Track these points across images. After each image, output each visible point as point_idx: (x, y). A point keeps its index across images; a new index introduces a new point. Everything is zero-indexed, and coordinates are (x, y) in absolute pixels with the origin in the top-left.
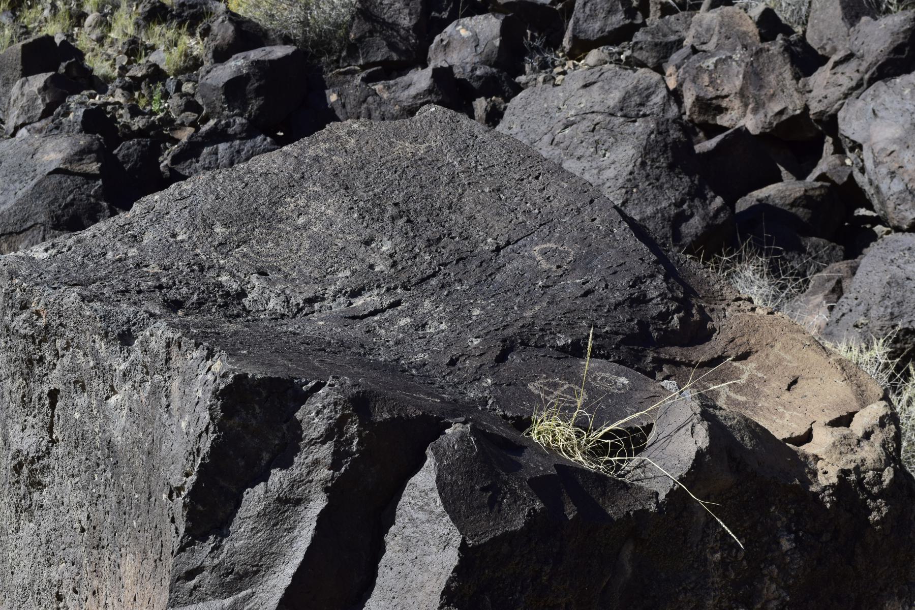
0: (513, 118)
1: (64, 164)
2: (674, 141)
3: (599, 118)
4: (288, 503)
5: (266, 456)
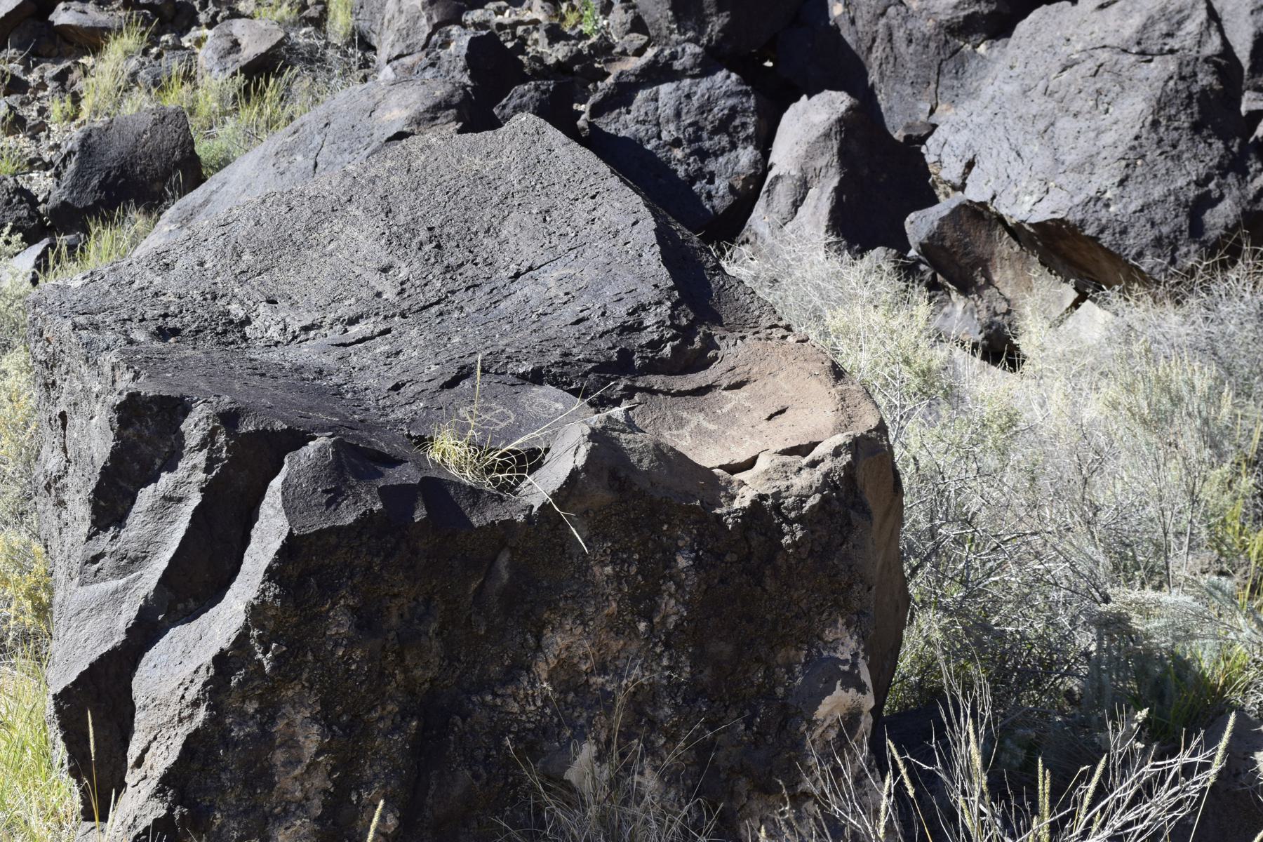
0: (1018, 51)
1: (409, 125)
2: (1203, 90)
3: (1103, 56)
4: (172, 500)
5: (158, 462)
